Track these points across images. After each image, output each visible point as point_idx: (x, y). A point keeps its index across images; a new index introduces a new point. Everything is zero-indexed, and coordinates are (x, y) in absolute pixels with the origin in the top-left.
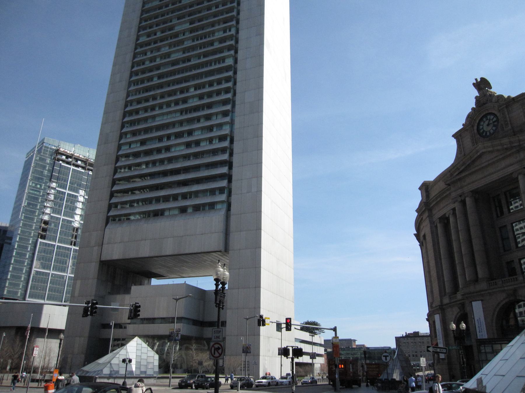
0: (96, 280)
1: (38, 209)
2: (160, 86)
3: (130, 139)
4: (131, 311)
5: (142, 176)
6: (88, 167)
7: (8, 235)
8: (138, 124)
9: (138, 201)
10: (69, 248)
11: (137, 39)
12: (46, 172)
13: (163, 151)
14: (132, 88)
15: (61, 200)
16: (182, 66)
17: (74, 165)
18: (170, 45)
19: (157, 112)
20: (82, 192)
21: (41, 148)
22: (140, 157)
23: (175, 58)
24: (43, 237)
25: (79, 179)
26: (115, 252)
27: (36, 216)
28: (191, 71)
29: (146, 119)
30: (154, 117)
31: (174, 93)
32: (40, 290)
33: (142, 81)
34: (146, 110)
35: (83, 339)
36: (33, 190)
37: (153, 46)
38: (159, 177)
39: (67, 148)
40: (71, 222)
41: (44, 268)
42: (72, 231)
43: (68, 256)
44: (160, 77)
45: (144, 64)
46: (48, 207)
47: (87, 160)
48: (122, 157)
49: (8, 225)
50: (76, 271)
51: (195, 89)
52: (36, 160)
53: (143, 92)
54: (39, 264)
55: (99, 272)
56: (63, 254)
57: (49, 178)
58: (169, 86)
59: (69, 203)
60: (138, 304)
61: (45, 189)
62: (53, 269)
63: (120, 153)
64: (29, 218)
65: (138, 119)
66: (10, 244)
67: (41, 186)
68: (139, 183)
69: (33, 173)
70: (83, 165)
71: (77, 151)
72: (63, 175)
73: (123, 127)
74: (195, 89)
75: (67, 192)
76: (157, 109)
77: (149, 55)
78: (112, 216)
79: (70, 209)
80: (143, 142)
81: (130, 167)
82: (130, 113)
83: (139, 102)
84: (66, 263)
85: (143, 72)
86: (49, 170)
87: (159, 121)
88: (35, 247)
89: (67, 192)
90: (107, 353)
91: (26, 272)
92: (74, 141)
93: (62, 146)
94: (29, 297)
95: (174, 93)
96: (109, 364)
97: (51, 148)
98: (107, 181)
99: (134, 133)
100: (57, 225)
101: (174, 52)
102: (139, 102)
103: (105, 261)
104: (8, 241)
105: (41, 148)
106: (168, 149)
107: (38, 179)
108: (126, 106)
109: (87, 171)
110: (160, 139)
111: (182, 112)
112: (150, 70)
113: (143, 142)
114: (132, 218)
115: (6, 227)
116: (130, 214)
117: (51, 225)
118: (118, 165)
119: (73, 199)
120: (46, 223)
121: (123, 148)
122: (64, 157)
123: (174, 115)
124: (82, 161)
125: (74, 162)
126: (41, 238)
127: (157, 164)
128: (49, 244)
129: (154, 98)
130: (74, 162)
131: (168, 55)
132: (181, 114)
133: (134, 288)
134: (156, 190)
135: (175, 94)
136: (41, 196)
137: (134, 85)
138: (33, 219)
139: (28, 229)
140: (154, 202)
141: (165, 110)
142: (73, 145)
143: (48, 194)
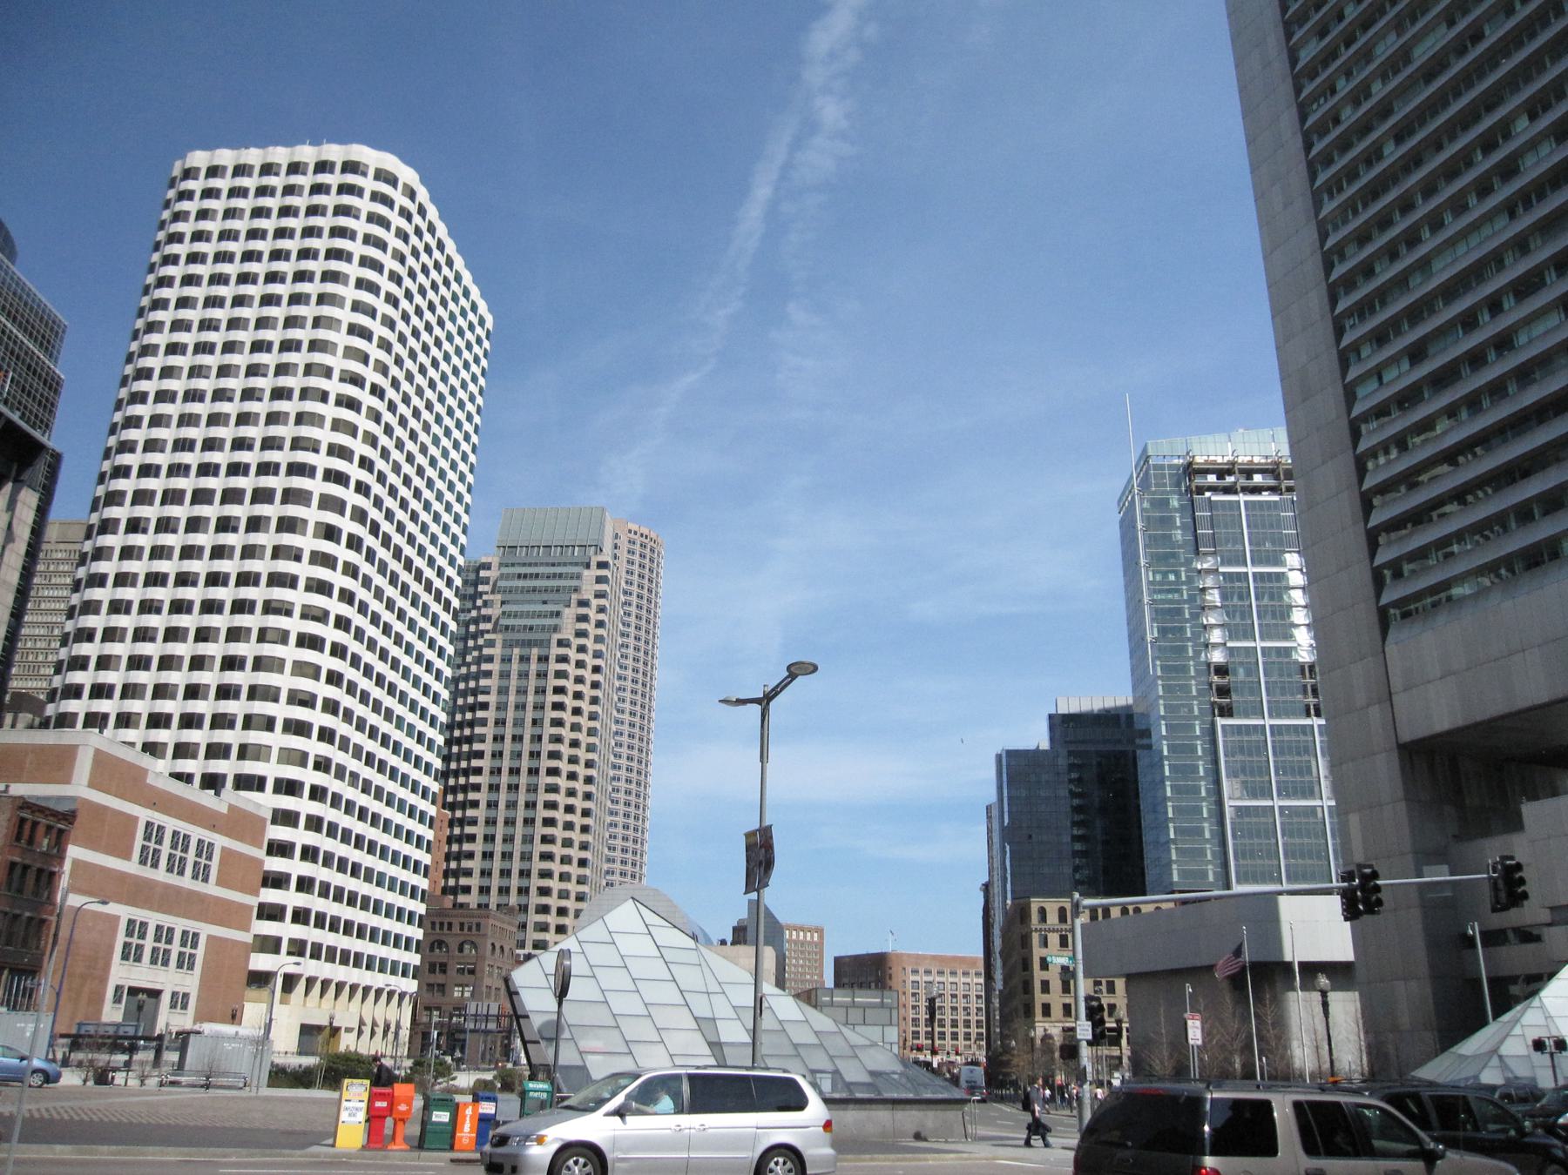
0: (1402, 806)
1: (1189, 639)
2: (1414, 160)
3: (1372, 357)
4: (1494, 884)
5: (1450, 457)
6: (1286, 483)
7: (1139, 726)
8: (1383, 303)
9: (1459, 536)
10: (1304, 726)
11: (1293, 60)
12: (1178, 535)
13: (1492, 356)
14: (1329, 207)
15: (1241, 598)
16: (1458, 66)
17: (1245, 490)
18: (1398, 26)
19: (1429, 244)
20: (1293, 559)
21: (1147, 473)
22: (1423, 399)
23: (1426, 58)
24: (1227, 712)
25: (1271, 526)
26: (1437, 710)
27: (1189, 659)
28: (1495, 65)
29: (1401, 282)
30: (1424, 265)
31: (1464, 160)
32: (1261, 857)
33: (1351, 174)
34: (1392, 253)
35: (1413, 984)
36: (1160, 592)
37: (1346, 55)
38: (1505, 441)
39: (1213, 450)
40: (1287, 652)
41: (1254, 796)
42: (1298, 677)
43: (1309, 750)
44: (1399, 136)
45: (1337, 121)
46: (1213, 626)
47: (1277, 464)
48: (1366, 421)
49: (1130, 701)
50: (1337, 792)
51: (1533, 117)
52: (1143, 510)
53: (1365, 206)
54: (1237, 786)
55: (1405, 783)
56: (1294, 746)
57: (1193, 548)
58: (1439, 147)
59: (1266, 601)
60: (1512, 858)
61: (1190, 580)
62: (1279, 795)
63: (1358, 410)
64: (1176, 669)
65: (1377, 289)
66: (1149, 747)
67: (1177, 574)
68: (1451, 478)
69: (1146, 546)
70: (1272, 482)
71: (1240, 451)
72: (1226, 527)
73: (1339, 332)
74: (1533, 117)
75: (1251, 570)
76: (1426, 234)
77: (1344, 87)
78: (1396, 604)
79: (1274, 616)
80: (1416, 354)
81: (1401, 442)
82: (1348, 283)
83: (1362, 238)
84: (1309, 772)
85: (1344, 145)
86: (1183, 527)
87: (1444, 269)
88: (1214, 742)
89: (1251, 570)
90: (1483, 1023)
91: (1210, 816)
92: (1224, 428)
93: (1196, 450)
94: (1238, 882)
95: (1464, 160)
96: (1495, 1061)
97: (1170, 467)
98: (1347, 504)
99: (1380, 337)
100: (1252, 670)
101: (1418, 38)
102: (1362, 238)
103: (1413, 742)
104: (1145, 741)
105: (1147, 473)
106: (1504, 343)
107: (1163, 560)
108: (1328, 267)
109: (1287, 496)
110: (1468, 321)
111: (1510, 209)
112: (1364, 128)
113: (1416, 354)
114: (1457, 591)
115: (1128, 707)
116: (1445, 585)
117: (1235, 675)
118: (1362, 447)
119: (1274, 586)
120: (1222, 670)
121: (1361, 392)
122: (1212, 479)
123: (1487, 231)
124: (1262, 471)
125: (1243, 482)
126: (1222, 715)
127: (1486, 403)
128: (1247, 726)
129: (1406, 206)
130: (1243, 482)
131: (1404, 55)
132: (1512, 215)
133: (1530, 811)
134: (1508, 485)
135: (1469, 164)
136: (1185, 602)
137: (1331, 197)
138: (1185, 669)
139: (1181, 698)
140: (1513, 525)
141: (1453, 226)
142: (1223, 437)
143: (1204, 590)
